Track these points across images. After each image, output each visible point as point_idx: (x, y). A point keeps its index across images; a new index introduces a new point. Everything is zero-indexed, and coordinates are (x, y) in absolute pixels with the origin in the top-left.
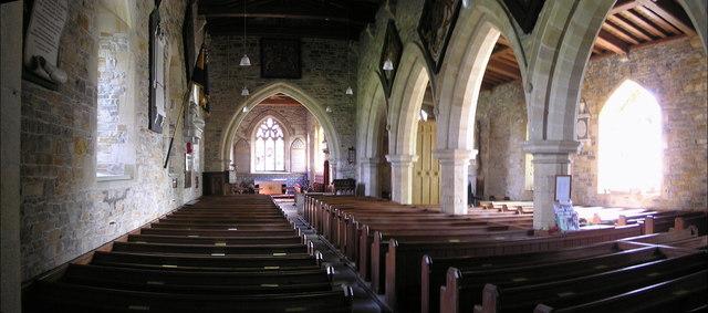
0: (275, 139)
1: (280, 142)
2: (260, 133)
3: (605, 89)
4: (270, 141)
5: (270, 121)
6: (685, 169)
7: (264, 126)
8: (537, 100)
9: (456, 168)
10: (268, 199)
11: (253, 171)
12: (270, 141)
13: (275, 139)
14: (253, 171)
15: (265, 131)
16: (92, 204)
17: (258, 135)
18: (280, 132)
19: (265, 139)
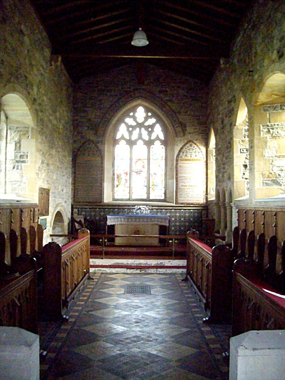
0: (149, 143)
1: (159, 149)
2: (122, 131)
3: (178, 257)
4: (140, 148)
5: (140, 113)
6: (105, 306)
7: (129, 121)
8: (204, 269)
9: (49, 41)
10: (113, 375)
11: (107, 199)
12: (140, 148)
13: (149, 143)
14: (107, 199)
15: (130, 129)
16: (171, 322)
17: (118, 136)
18: (158, 131)
19: (131, 143)
